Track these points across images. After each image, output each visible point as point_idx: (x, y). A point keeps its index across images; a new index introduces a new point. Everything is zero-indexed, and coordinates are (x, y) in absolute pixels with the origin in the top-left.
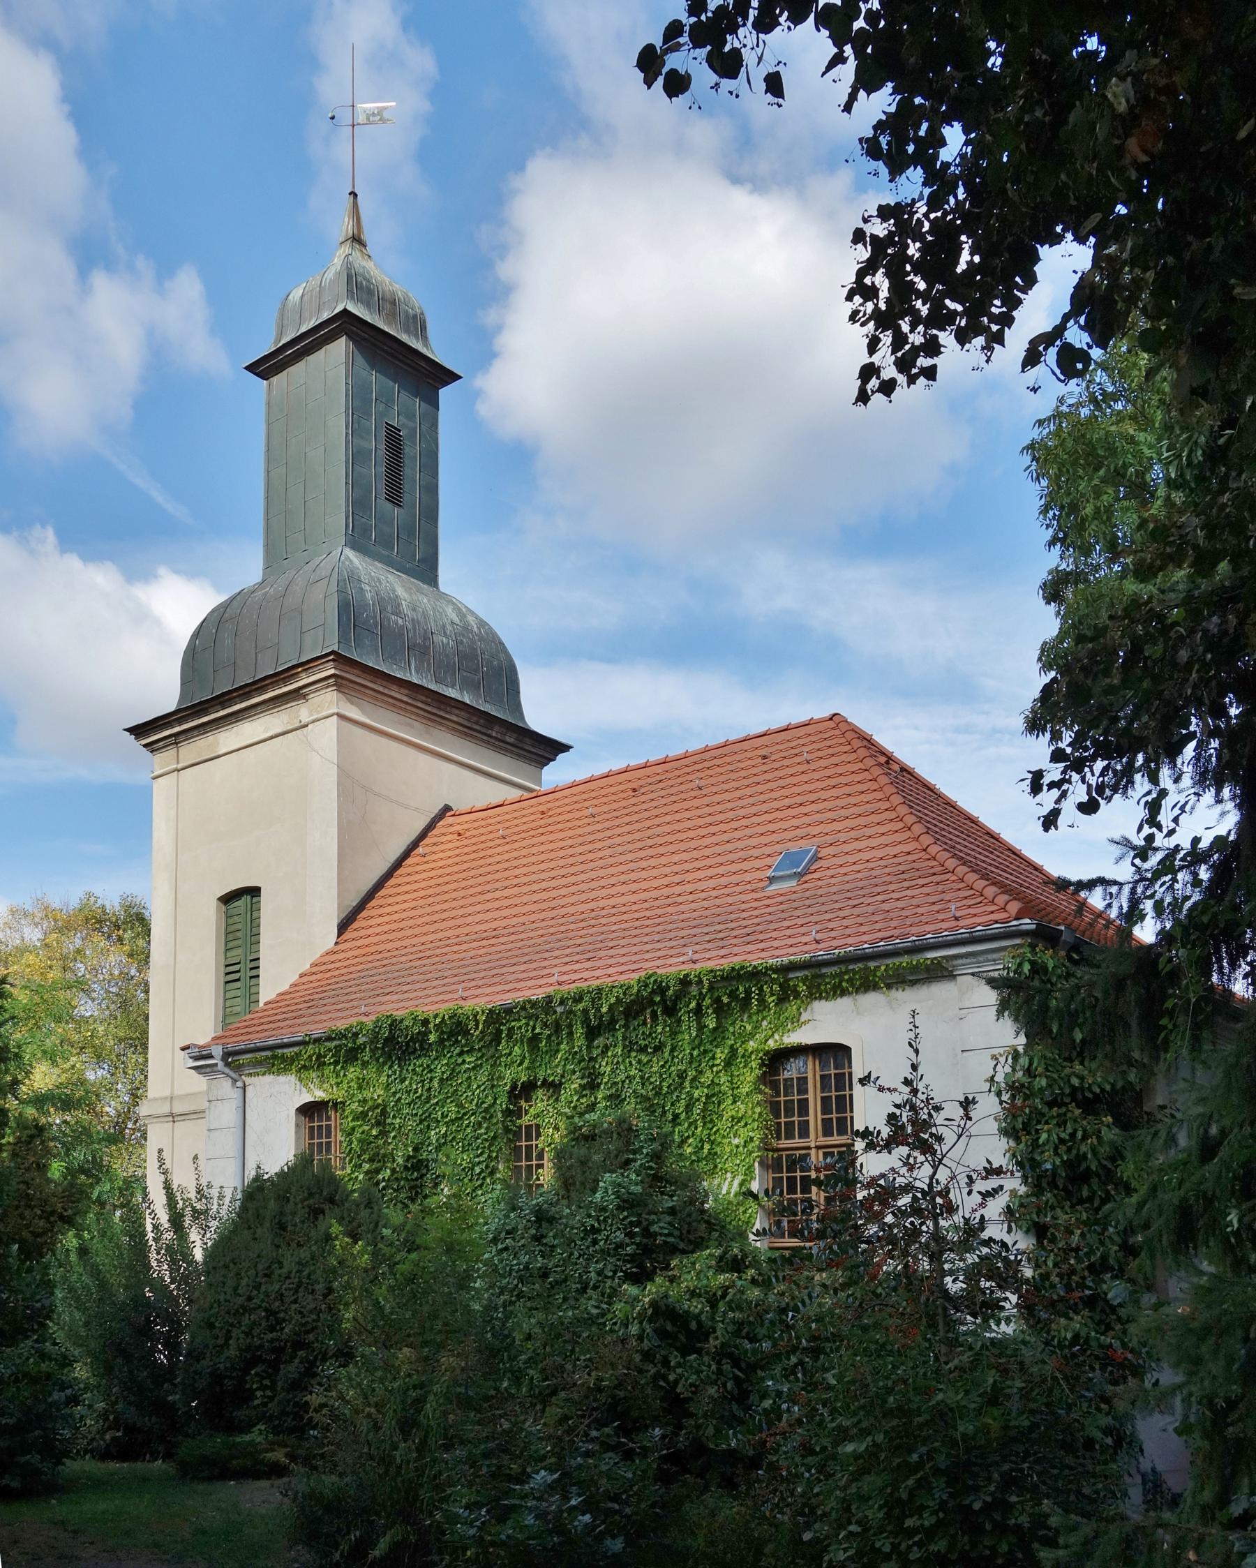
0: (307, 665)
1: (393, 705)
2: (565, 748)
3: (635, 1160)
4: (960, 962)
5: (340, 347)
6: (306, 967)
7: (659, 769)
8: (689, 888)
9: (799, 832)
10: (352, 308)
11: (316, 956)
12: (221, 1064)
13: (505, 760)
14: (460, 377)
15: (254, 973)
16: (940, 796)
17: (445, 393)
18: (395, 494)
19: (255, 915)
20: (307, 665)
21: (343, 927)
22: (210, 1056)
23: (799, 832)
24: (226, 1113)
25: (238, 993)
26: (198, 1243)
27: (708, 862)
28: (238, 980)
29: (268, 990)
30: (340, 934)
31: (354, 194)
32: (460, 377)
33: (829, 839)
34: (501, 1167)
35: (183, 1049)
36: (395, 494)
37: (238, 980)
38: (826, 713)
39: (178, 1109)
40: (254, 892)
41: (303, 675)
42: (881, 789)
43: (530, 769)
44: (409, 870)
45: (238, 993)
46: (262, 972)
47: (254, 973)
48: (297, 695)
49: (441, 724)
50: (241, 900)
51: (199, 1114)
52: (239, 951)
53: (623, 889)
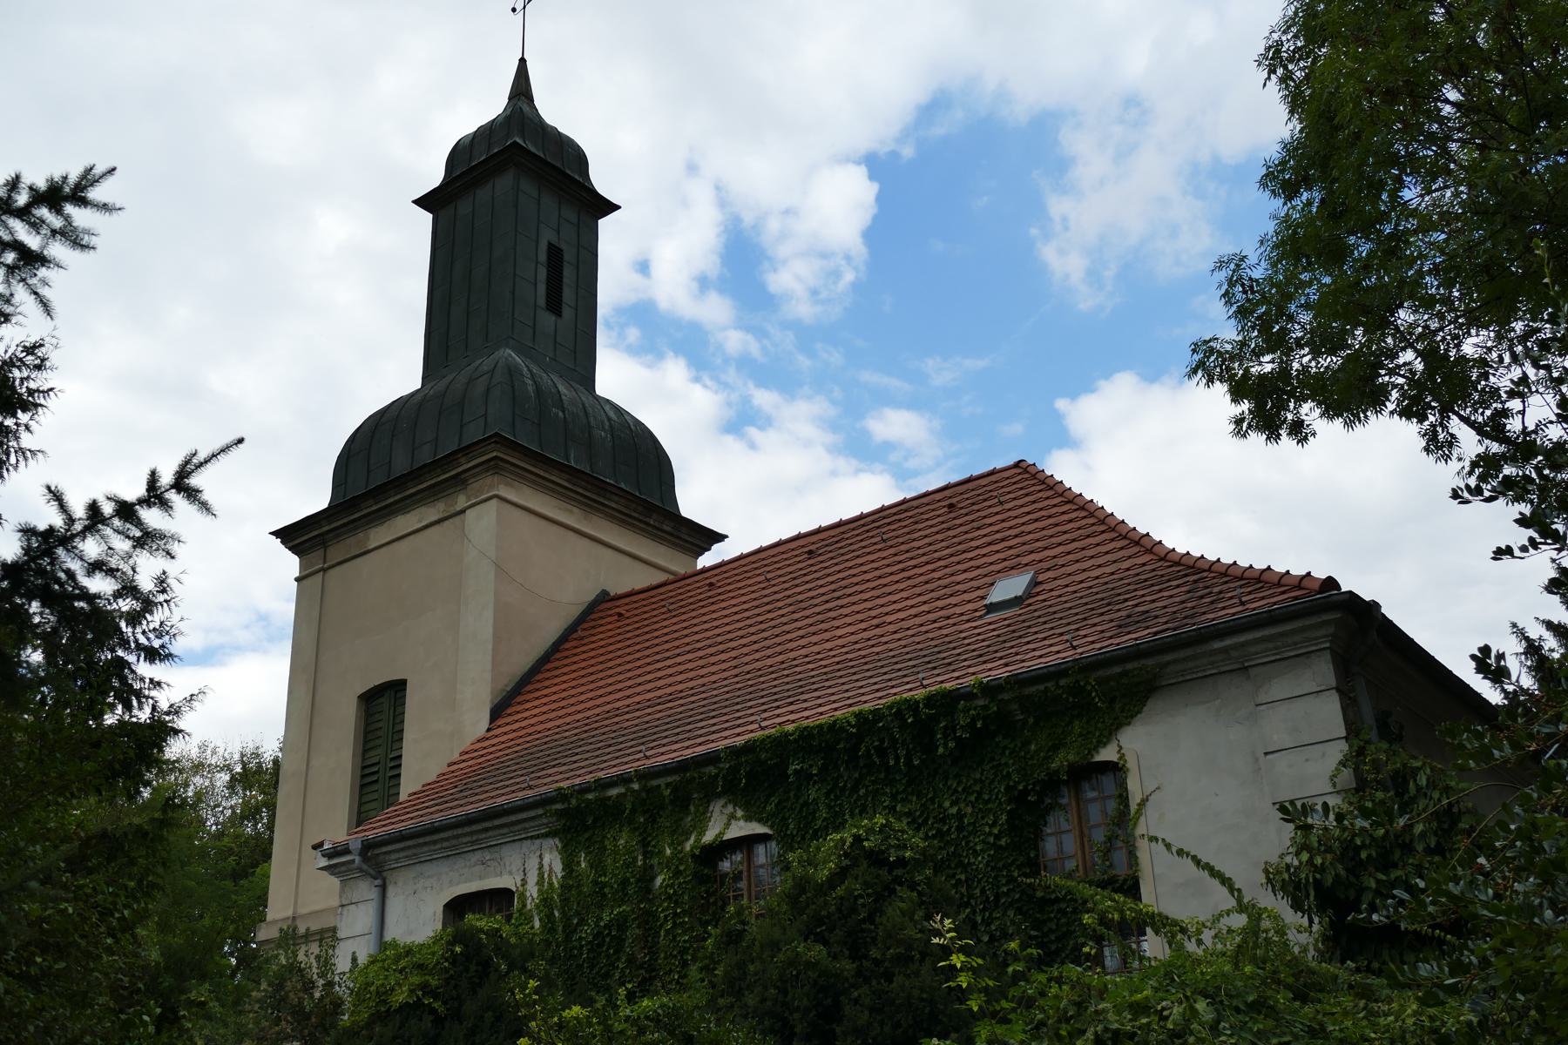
0: (466, 450)
1: (553, 491)
4: (1253, 649)
5: (504, 183)
6: (456, 757)
7: (832, 533)
8: (892, 628)
10: (520, 141)
11: (466, 744)
12: (357, 859)
13: (662, 549)
15: (394, 772)
17: (605, 224)
18: (554, 304)
19: (399, 710)
20: (466, 450)
21: (496, 713)
22: (347, 851)
25: (375, 796)
26: (1510, 376)
27: (909, 603)
28: (376, 782)
29: (409, 785)
30: (492, 720)
31: (523, 61)
32: (618, 207)
33: (1045, 565)
35: (315, 847)
36: (554, 304)
37: (376, 782)
38: (1011, 462)
41: (462, 460)
43: (688, 559)
44: (556, 664)
45: (375, 796)
46: (404, 771)
47: (394, 772)
48: (460, 482)
49: (598, 510)
52: (379, 751)
53: (814, 639)
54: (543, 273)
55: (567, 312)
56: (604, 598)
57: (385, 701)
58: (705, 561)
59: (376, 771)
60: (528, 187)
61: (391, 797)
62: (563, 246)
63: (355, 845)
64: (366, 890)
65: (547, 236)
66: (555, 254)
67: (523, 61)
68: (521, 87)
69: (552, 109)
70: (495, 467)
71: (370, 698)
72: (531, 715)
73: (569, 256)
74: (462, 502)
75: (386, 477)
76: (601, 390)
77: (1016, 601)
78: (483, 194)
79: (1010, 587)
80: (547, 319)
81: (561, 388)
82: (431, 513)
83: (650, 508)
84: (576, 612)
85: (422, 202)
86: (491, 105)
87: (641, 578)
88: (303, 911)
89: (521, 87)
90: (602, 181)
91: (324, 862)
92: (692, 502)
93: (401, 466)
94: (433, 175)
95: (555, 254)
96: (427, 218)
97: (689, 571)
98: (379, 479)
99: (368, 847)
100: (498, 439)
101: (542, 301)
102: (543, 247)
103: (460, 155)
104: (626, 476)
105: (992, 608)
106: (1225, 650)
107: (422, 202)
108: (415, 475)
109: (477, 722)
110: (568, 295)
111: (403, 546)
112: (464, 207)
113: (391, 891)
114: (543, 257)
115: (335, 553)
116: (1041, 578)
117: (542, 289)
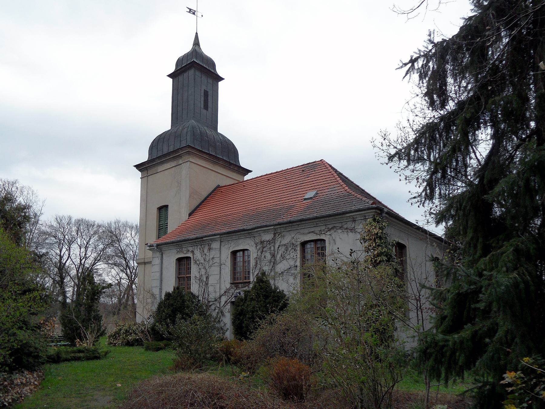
2: (251, 171)
3: (492, 332)
5: (191, 72)
8: (282, 202)
9: (312, 188)
14: (223, 79)
16: (349, 180)
17: (220, 83)
18: (206, 107)
20: (181, 149)
21: (190, 215)
23: (312, 188)
24: (157, 261)
29: (169, 231)
31: (197, 33)
32: (223, 79)
34: (500, 321)
36: (206, 107)
39: (146, 261)
40: (166, 206)
42: (334, 177)
48: (180, 156)
50: (163, 209)
51: (150, 263)
54: (203, 99)
55: (209, 109)
56: (218, 186)
57: (163, 210)
58: (247, 178)
59: (162, 228)
60: (198, 74)
61: (165, 233)
62: (208, 90)
63: (155, 245)
64: (158, 254)
65: (204, 88)
66: (206, 94)
67: (197, 33)
68: (196, 43)
69: (206, 50)
70: (189, 153)
71: (160, 209)
72: (198, 216)
73: (210, 93)
74: (181, 162)
75: (162, 155)
76: (219, 131)
77: (311, 198)
78: (185, 75)
79: (311, 194)
80: (205, 111)
81: (207, 131)
82: (173, 164)
83: (231, 164)
84: (211, 190)
85: (170, 76)
86: (188, 48)
87: (229, 182)
88: (146, 257)
89: (196, 43)
90: (220, 71)
91: (148, 248)
92: (244, 163)
93: (165, 151)
94: (172, 69)
95: (206, 94)
96: (171, 80)
97: (242, 181)
98: (160, 154)
99: (158, 245)
100: (189, 146)
101: (202, 106)
102: (203, 91)
103: (179, 62)
104: (224, 154)
105: (305, 199)
106: (349, 216)
107: (170, 76)
108: (169, 154)
109: (185, 216)
110: (210, 105)
111: (165, 173)
112: (181, 78)
113: (164, 255)
114: (203, 94)
115: (150, 172)
116: (319, 192)
117: (202, 102)
